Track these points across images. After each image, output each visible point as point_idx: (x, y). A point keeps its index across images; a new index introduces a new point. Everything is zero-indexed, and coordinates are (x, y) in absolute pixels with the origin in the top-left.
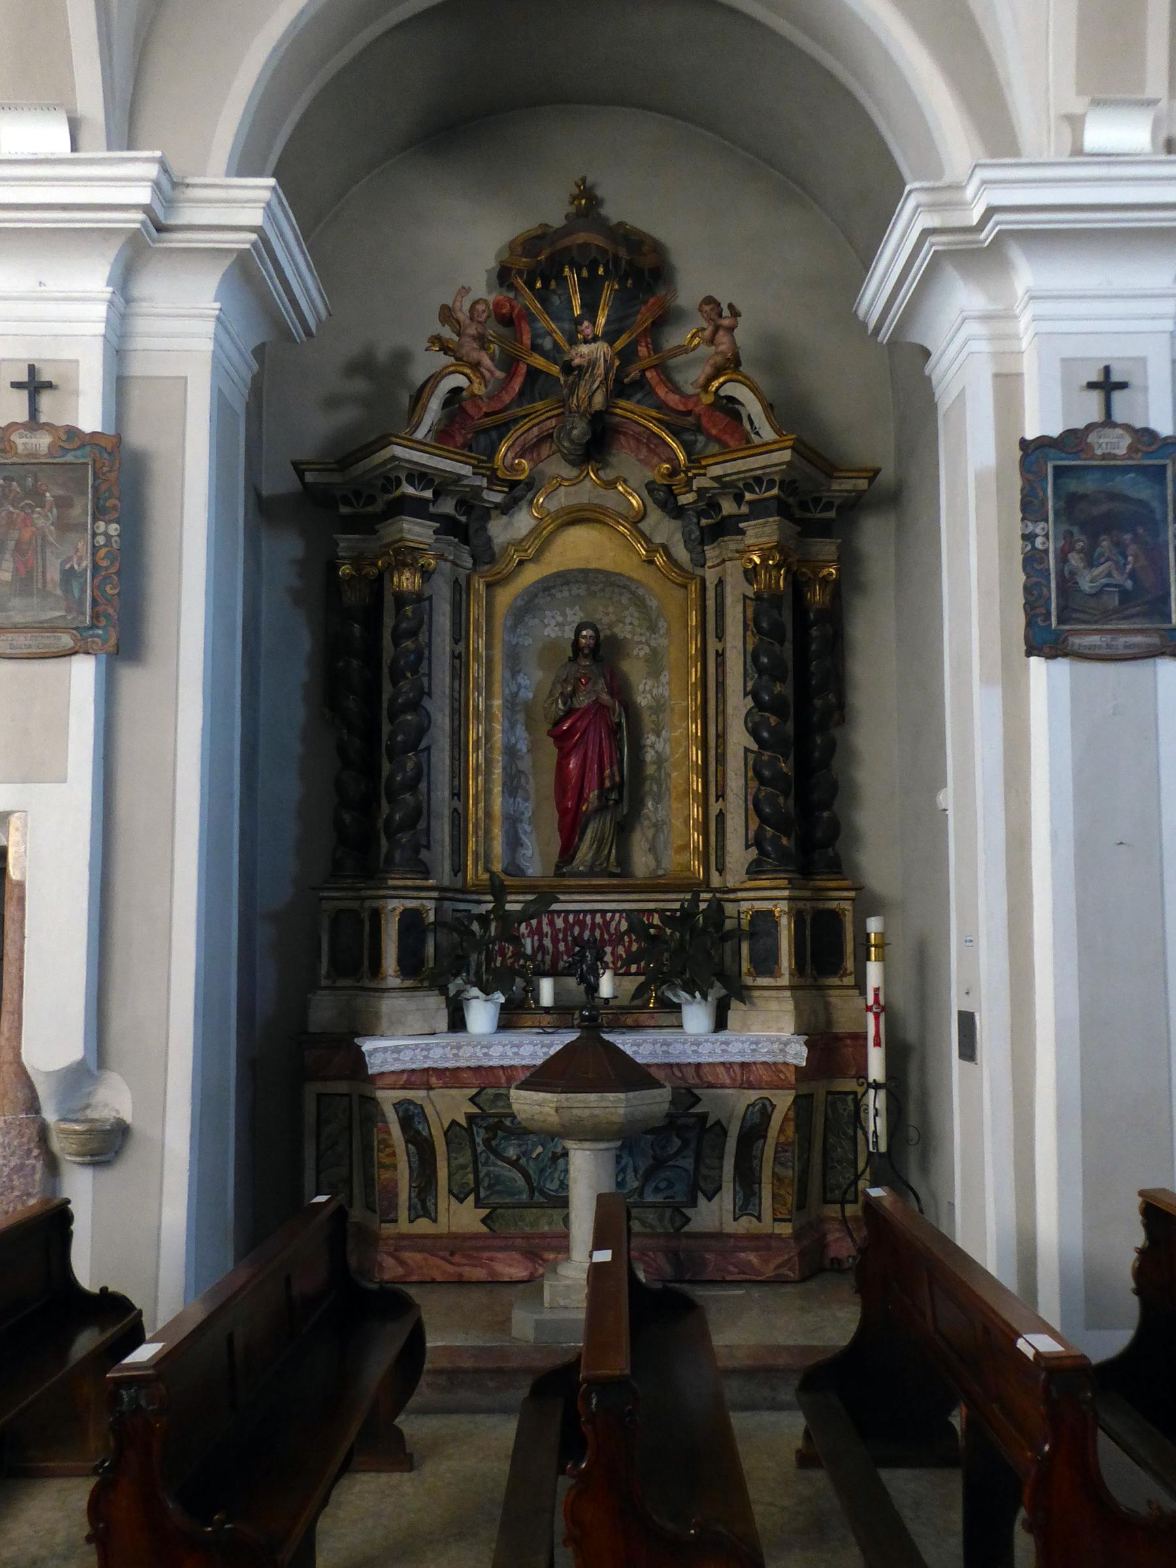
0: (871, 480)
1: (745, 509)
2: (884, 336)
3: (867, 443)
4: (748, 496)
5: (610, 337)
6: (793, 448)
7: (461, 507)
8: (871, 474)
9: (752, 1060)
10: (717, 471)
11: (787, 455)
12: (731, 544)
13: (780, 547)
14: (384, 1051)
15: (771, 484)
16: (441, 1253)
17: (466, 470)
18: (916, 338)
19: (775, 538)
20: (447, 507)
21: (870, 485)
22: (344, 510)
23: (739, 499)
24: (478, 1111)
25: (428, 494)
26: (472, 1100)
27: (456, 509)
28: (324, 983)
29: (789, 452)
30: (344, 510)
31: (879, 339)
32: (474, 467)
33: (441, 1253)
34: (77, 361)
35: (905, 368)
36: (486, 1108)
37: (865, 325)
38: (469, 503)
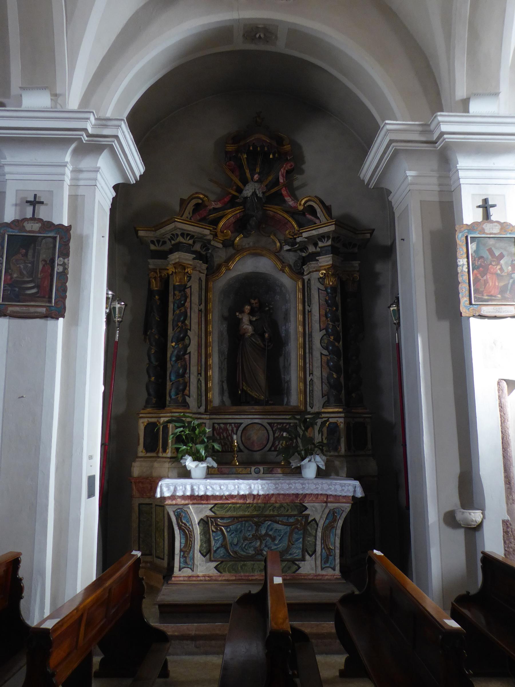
0: (371, 234)
1: (318, 249)
2: (372, 186)
3: (365, 214)
4: (320, 244)
5: (260, 181)
6: (335, 224)
7: (203, 248)
8: (370, 232)
9: (340, 494)
10: (305, 235)
11: (332, 228)
12: (313, 265)
13: (333, 266)
14: (167, 487)
15: (328, 238)
16: (238, 505)
17: (207, 232)
18: (383, 185)
19: (331, 262)
20: (197, 247)
21: (371, 236)
22: (152, 247)
23: (316, 245)
24: (213, 514)
25: (191, 242)
26: (211, 510)
27: (201, 248)
28: (140, 454)
29: (334, 226)
30: (152, 247)
31: (370, 187)
32: (210, 230)
33: (238, 505)
34: (52, 191)
35: (380, 196)
36: (217, 512)
37: (363, 181)
38: (206, 245)
